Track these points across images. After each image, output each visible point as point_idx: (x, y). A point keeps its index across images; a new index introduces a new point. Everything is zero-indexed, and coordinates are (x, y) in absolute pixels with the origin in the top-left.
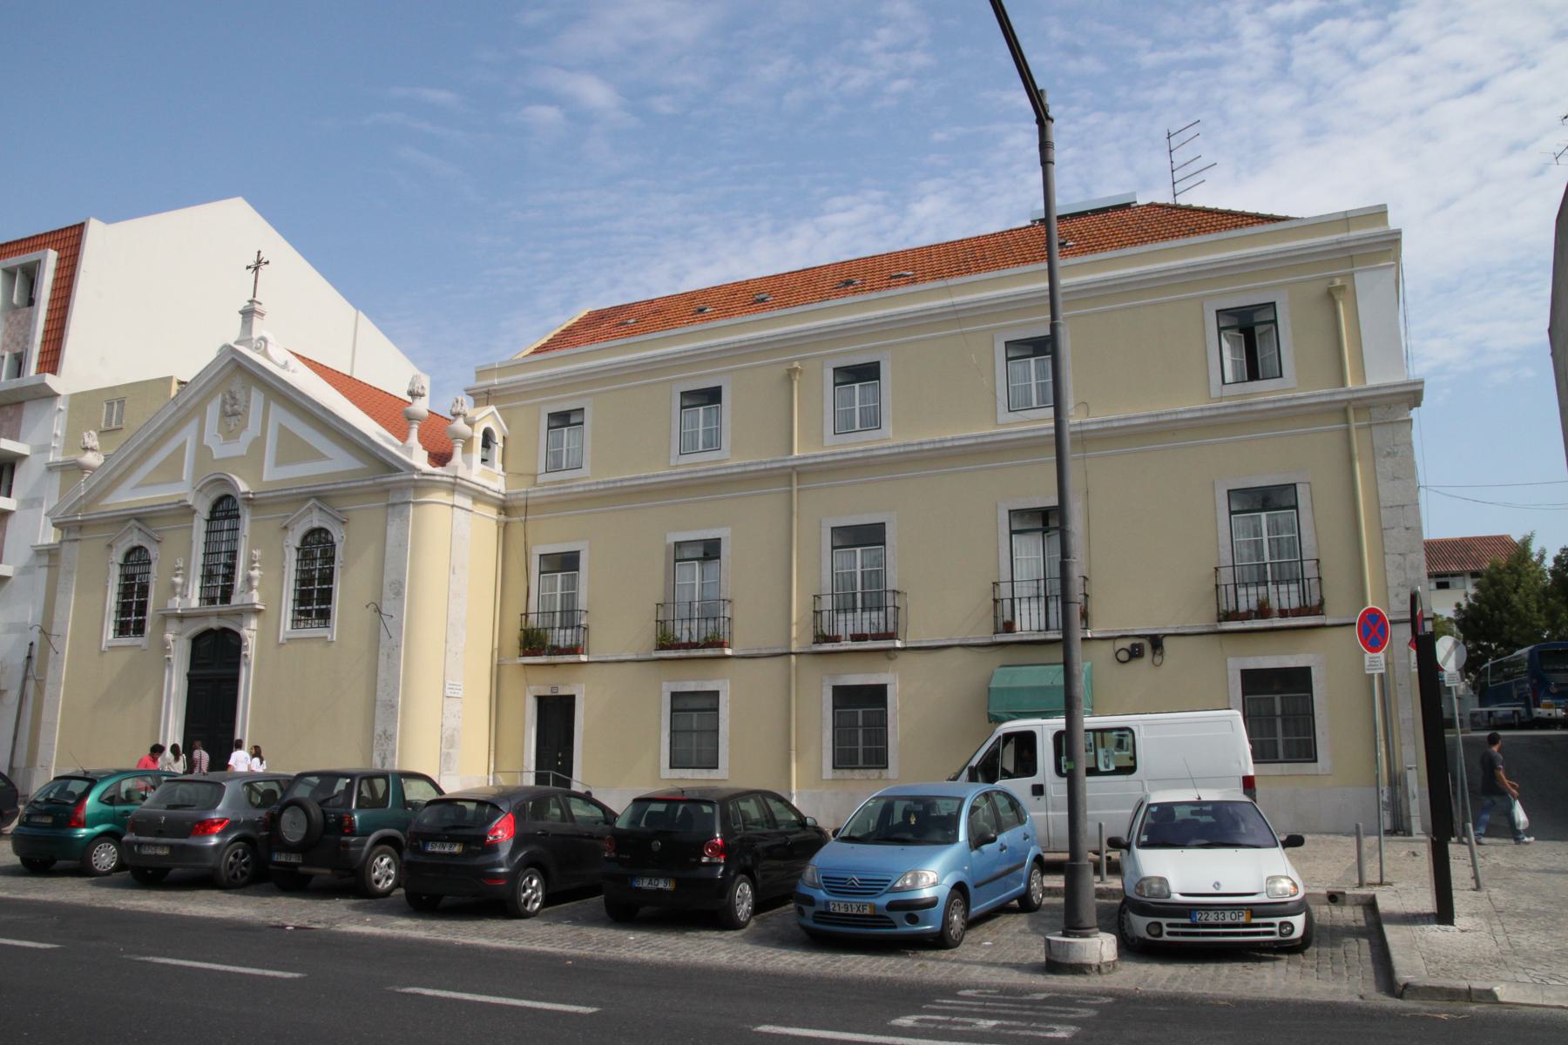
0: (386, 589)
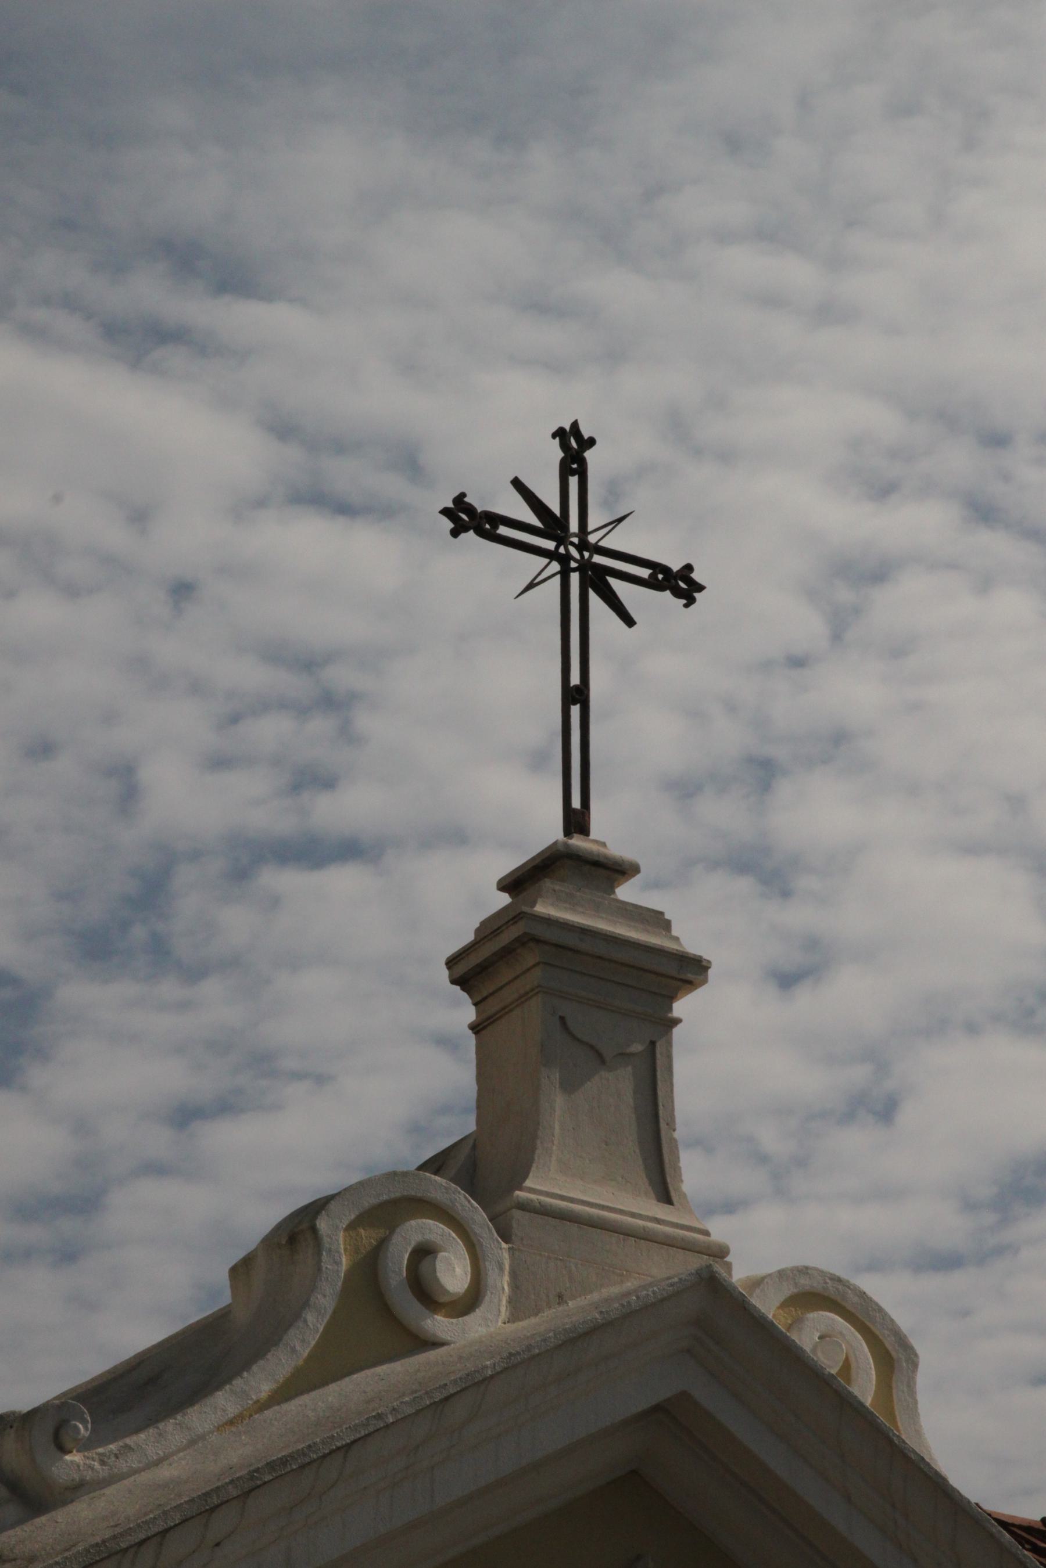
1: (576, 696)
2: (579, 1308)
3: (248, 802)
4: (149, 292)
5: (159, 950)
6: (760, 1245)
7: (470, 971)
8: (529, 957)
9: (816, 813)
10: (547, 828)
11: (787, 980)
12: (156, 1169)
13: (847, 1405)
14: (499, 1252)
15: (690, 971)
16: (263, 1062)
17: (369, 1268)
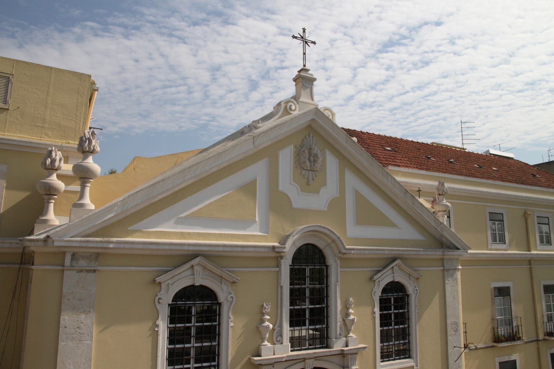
0: (449, 328)
1: (304, 54)
2: (305, 111)
3: (276, 64)
4: (265, 15)
5: (269, 77)
6: (321, 106)
7: (295, 80)
8: (300, 78)
9: (329, 64)
10: (302, 67)
11: (327, 80)
12: (269, 98)
13: (329, 119)
14: (298, 106)
15: (315, 79)
16: (279, 88)
17: (286, 107)
